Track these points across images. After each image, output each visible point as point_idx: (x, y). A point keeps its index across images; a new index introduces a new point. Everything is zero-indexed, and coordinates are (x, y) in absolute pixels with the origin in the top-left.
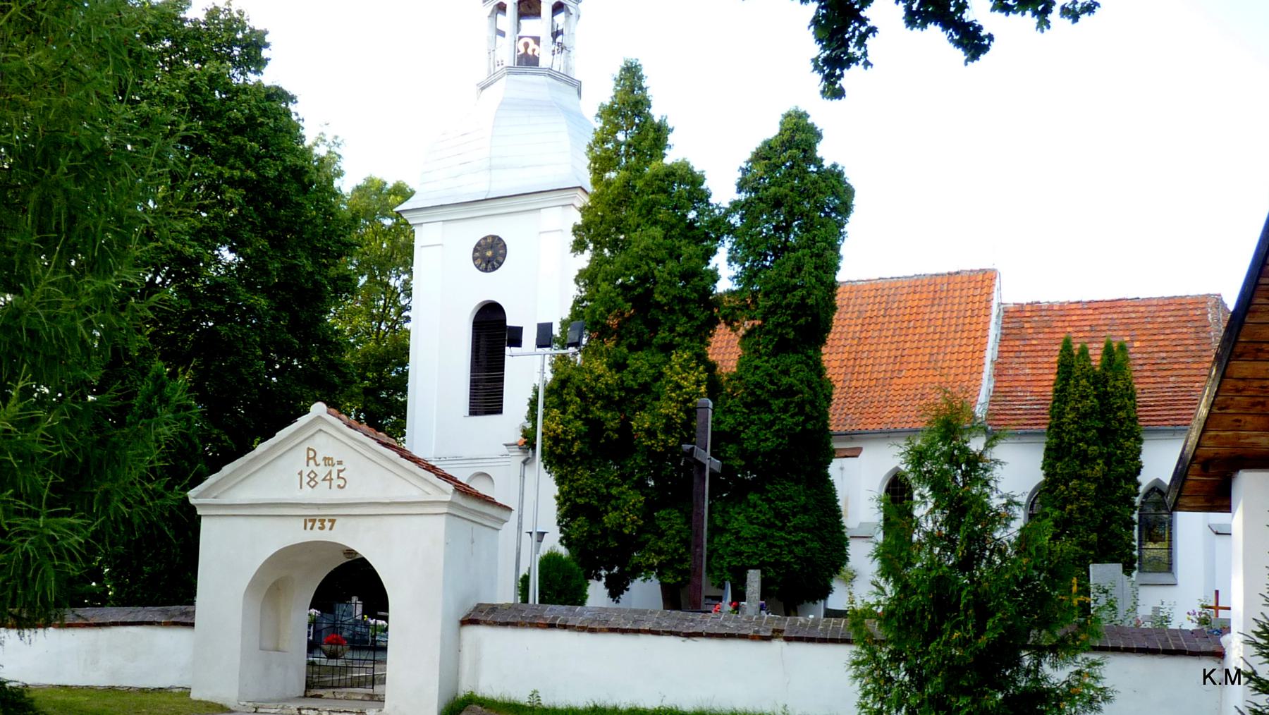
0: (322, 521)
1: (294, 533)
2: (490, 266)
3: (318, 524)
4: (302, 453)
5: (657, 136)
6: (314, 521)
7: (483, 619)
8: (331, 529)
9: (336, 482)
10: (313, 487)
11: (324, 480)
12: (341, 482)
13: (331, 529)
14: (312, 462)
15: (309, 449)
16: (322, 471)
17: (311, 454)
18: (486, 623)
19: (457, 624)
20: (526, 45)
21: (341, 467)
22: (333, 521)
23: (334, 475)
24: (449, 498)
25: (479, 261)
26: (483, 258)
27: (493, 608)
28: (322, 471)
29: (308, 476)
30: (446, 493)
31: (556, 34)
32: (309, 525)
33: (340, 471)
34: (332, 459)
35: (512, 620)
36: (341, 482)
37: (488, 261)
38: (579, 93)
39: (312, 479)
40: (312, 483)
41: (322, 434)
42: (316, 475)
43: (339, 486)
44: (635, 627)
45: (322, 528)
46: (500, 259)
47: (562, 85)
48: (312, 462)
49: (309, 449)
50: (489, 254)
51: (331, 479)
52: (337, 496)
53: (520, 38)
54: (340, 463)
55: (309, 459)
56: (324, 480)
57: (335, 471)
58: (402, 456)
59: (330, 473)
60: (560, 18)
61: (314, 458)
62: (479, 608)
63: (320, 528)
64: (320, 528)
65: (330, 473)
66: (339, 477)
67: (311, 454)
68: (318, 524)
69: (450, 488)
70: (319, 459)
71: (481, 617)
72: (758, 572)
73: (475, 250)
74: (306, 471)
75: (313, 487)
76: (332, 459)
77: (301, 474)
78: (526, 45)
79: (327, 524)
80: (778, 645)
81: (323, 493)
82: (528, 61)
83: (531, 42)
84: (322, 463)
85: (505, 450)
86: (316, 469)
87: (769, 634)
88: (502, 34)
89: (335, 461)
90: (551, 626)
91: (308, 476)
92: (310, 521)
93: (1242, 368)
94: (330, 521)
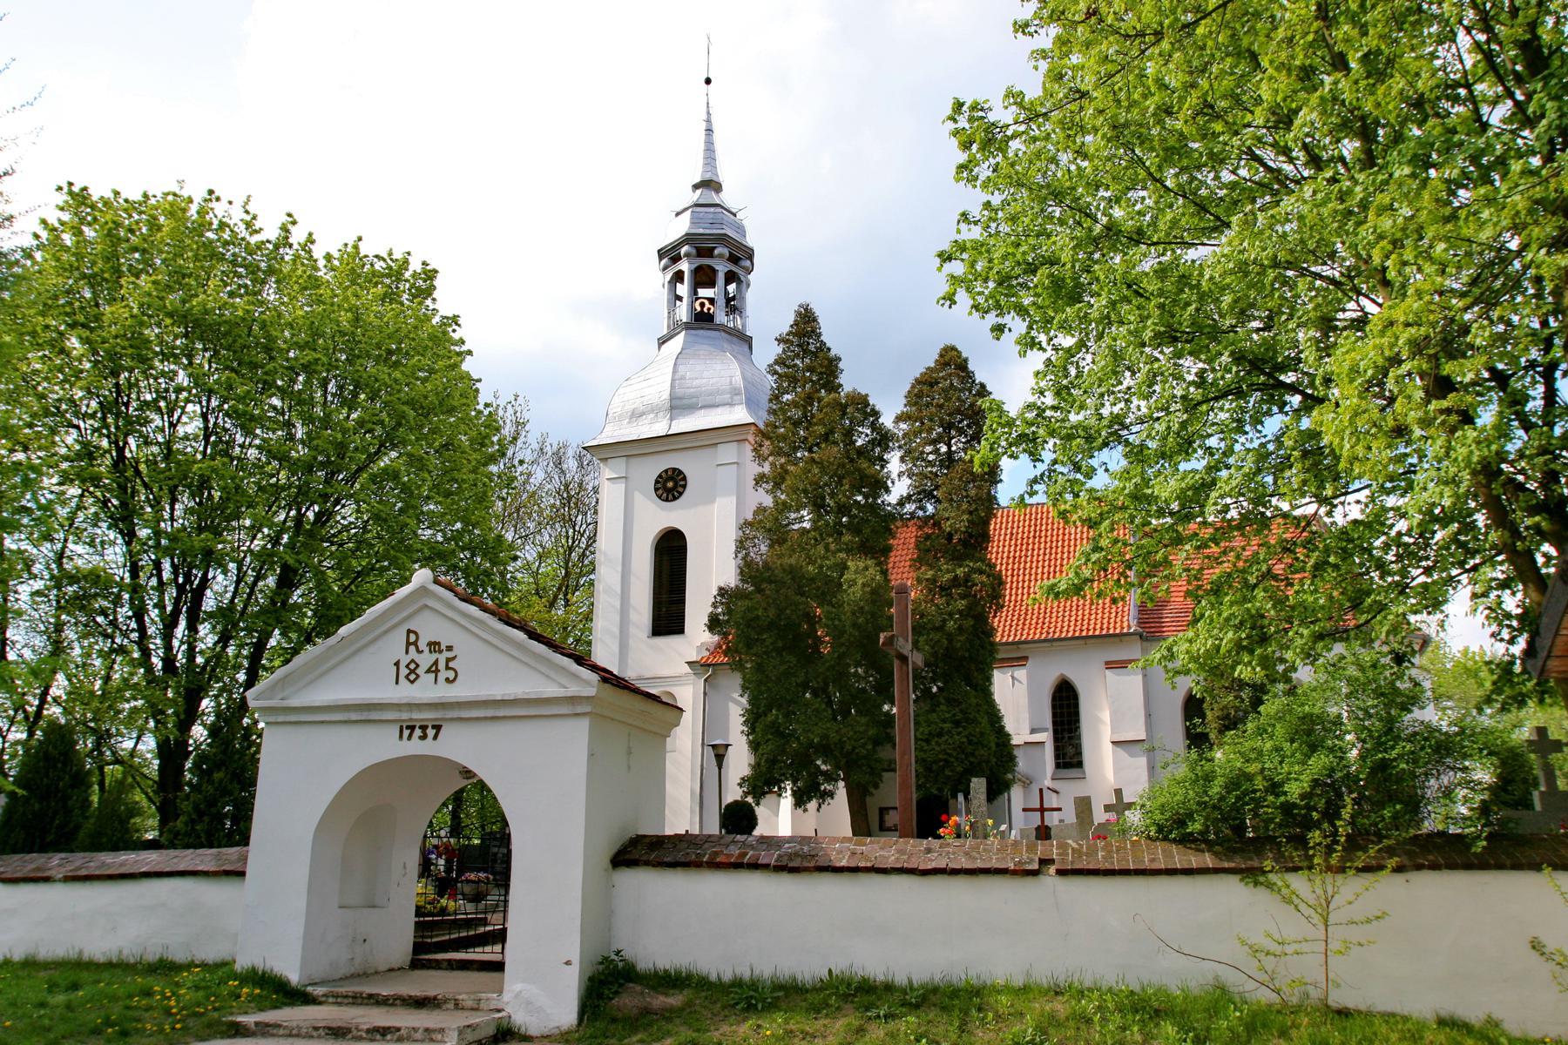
0: (423, 728)
1: (386, 745)
2: (670, 497)
3: (418, 732)
4: (399, 638)
5: (827, 368)
6: (412, 728)
7: (644, 858)
8: (435, 737)
9: (443, 674)
10: (412, 682)
11: (428, 671)
12: (451, 675)
13: (435, 737)
14: (412, 648)
15: (409, 631)
16: (426, 660)
17: (413, 638)
18: (647, 863)
19: (606, 861)
20: (702, 305)
21: (450, 655)
22: (438, 728)
23: (442, 665)
24: (591, 691)
25: (660, 492)
26: (669, 491)
27: (659, 842)
28: (426, 660)
29: (407, 666)
30: (587, 683)
31: (728, 300)
32: (406, 733)
33: (448, 660)
34: (439, 644)
35: (683, 860)
36: (451, 675)
37: (669, 491)
38: (750, 348)
39: (412, 671)
40: (412, 677)
41: (426, 614)
42: (418, 666)
43: (447, 680)
44: (853, 865)
45: (424, 737)
46: (680, 489)
47: (735, 339)
48: (412, 648)
49: (409, 631)
50: (670, 484)
51: (437, 671)
52: (443, 692)
53: (697, 299)
54: (450, 648)
55: (408, 644)
56: (428, 671)
57: (443, 661)
58: (530, 638)
59: (436, 663)
60: (732, 288)
61: (415, 644)
62: (637, 841)
63: (420, 738)
64: (420, 738)
65: (436, 663)
66: (448, 668)
67: (413, 638)
68: (418, 732)
69: (594, 677)
70: (422, 645)
71: (635, 855)
72: (983, 781)
73: (657, 482)
74: (405, 660)
75: (412, 682)
76: (439, 644)
77: (397, 664)
78: (702, 305)
79: (431, 732)
80: (1050, 881)
81: (426, 690)
82: (702, 319)
83: (706, 302)
84: (426, 649)
85: (687, 669)
86: (418, 658)
87: (1035, 866)
88: (680, 298)
89: (443, 647)
90: (737, 866)
91: (407, 666)
92: (408, 727)
93: (505, 851)
94: (434, 727)
